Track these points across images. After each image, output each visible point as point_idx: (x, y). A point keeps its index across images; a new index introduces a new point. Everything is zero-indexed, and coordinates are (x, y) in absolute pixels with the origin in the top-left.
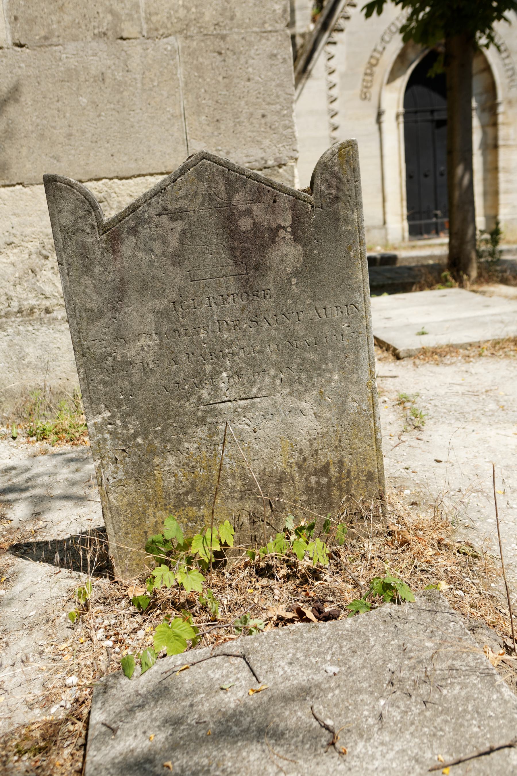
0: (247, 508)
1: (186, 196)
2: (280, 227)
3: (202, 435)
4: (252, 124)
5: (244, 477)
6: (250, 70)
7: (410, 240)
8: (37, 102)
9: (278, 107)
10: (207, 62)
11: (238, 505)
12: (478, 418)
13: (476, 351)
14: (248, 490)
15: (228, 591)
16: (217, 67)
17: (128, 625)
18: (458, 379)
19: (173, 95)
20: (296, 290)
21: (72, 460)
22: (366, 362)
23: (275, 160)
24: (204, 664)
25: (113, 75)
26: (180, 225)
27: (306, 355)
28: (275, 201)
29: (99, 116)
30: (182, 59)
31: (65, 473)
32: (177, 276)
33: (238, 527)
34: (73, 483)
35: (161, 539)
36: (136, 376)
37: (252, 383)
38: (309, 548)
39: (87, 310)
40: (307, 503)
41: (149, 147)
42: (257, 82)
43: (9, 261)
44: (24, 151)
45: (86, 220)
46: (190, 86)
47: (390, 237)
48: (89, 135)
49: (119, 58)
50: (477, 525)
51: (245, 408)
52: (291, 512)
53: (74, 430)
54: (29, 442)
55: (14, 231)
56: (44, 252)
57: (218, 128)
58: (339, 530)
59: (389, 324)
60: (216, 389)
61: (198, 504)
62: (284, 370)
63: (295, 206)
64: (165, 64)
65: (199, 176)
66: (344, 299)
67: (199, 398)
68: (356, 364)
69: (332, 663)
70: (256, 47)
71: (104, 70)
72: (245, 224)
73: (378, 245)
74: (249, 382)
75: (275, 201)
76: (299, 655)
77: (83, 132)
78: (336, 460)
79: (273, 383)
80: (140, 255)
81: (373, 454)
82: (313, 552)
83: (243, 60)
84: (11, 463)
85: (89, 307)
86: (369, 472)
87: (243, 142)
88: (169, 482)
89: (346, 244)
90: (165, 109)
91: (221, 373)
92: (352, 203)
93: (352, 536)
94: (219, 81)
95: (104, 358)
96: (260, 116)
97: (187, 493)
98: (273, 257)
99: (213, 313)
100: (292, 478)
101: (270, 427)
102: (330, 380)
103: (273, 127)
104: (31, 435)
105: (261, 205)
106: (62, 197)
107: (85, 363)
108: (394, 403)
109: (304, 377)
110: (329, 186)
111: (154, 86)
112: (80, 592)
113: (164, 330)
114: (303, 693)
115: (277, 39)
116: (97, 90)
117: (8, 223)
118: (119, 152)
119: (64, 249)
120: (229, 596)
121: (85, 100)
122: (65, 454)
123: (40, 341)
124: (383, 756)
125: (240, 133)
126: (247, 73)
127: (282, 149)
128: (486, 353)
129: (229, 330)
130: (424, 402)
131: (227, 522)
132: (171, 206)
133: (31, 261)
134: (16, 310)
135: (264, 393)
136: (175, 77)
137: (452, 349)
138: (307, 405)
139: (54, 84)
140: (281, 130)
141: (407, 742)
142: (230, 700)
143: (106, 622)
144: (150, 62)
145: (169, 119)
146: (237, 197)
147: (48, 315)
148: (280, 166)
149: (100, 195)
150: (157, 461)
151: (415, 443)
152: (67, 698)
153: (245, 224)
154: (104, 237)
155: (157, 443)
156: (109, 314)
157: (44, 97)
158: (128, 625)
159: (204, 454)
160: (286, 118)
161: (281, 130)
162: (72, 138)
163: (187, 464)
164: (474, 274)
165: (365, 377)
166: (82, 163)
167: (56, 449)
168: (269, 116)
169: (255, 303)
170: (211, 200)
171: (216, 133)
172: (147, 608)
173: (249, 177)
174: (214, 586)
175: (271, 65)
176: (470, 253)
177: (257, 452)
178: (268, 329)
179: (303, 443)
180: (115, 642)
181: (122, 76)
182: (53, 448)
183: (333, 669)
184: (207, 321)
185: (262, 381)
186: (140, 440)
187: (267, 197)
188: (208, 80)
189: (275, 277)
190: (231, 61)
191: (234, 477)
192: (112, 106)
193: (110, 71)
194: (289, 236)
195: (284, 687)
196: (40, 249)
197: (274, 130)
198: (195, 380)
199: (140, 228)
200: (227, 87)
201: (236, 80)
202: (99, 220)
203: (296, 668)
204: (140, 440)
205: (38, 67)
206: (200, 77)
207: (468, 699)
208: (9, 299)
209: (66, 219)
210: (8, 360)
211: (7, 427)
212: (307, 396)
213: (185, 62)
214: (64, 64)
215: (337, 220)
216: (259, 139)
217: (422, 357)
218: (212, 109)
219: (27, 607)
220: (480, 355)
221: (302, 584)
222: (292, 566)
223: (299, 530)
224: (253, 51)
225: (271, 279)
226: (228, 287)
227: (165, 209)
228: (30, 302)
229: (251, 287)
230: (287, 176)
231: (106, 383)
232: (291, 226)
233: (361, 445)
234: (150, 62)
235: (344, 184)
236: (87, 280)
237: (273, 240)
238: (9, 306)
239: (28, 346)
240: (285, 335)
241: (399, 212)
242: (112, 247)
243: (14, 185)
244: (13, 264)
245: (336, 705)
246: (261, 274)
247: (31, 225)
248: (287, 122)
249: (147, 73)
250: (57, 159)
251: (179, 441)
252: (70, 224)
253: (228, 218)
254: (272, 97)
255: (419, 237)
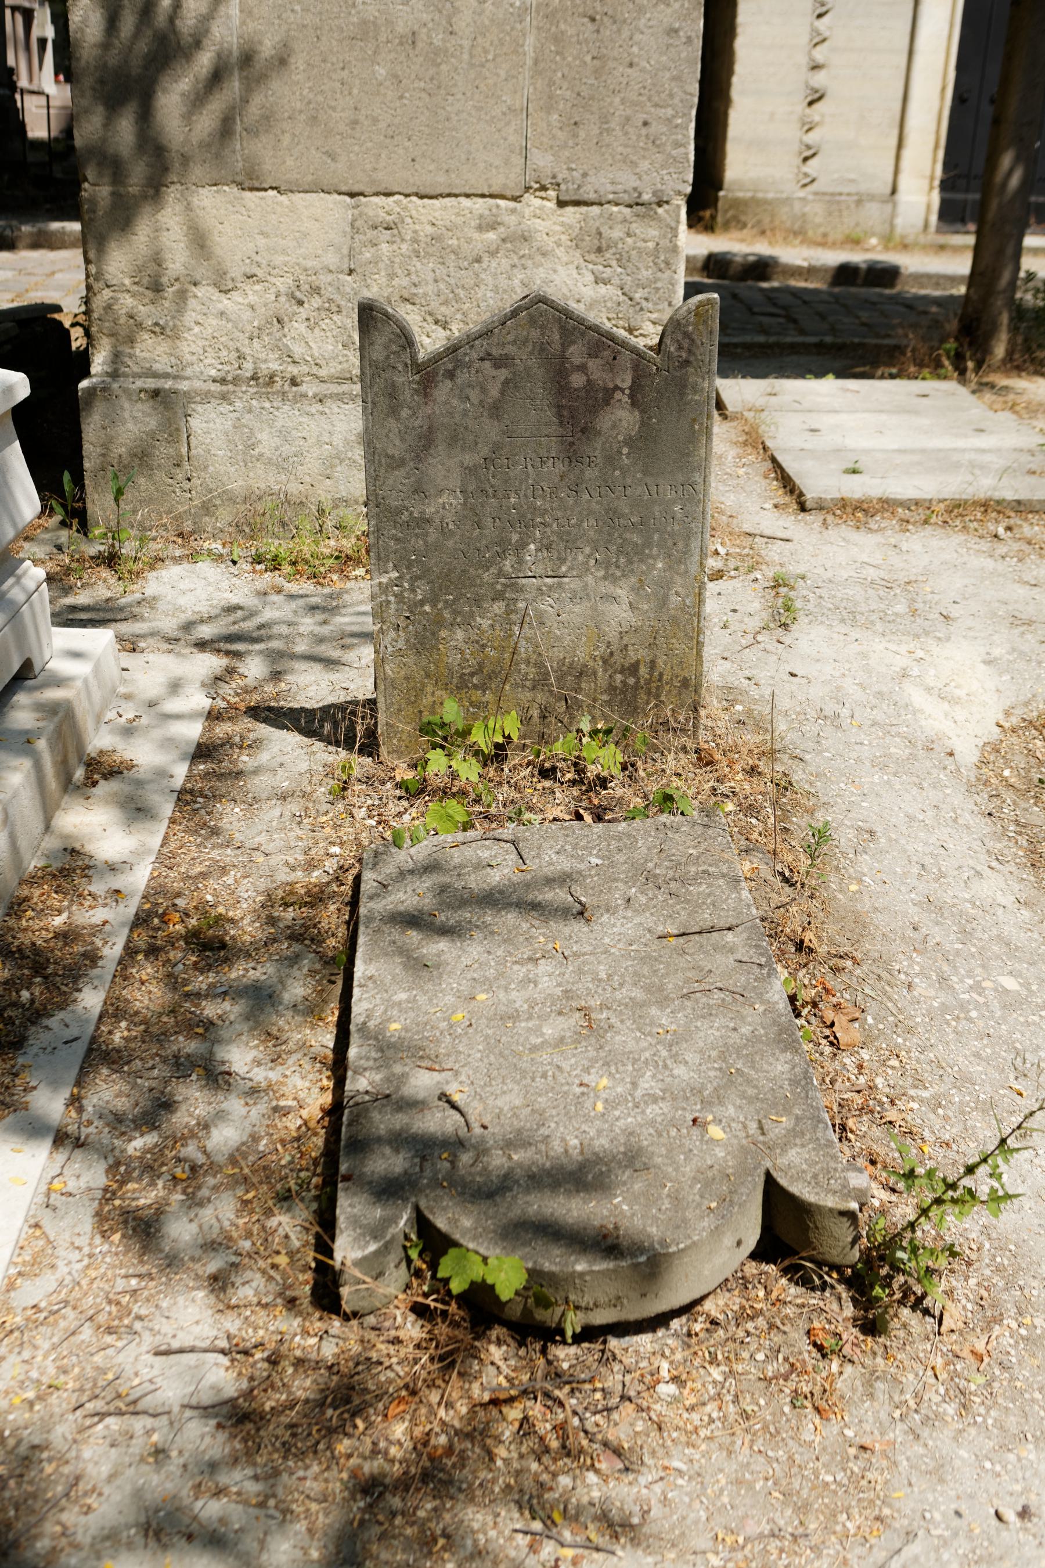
0: (539, 700)
1: (514, 342)
2: (617, 388)
3: (498, 612)
4: (626, 133)
5: (539, 665)
6: (635, 49)
7: (938, 231)
8: (313, 66)
9: (670, 112)
10: (571, 31)
11: (529, 695)
12: (872, 623)
13: (922, 513)
14: (541, 681)
15: (505, 787)
16: (586, 40)
17: (393, 808)
18: (877, 558)
19: (513, 77)
20: (626, 461)
21: (314, 608)
22: (698, 552)
23: (654, 193)
24: (474, 844)
25: (429, 37)
26: (503, 374)
27: (628, 536)
28: (615, 358)
29: (401, 97)
30: (534, 23)
31: (308, 624)
32: (492, 430)
33: (526, 720)
34: (321, 640)
35: (439, 721)
36: (433, 536)
37: (563, 560)
38: (601, 753)
39: (387, 456)
40: (608, 703)
41: (469, 153)
42: (643, 70)
43: (246, 302)
44: (286, 139)
45: (399, 357)
46: (542, 65)
47: (899, 221)
48: (382, 125)
49: (440, 12)
50: (807, 757)
51: (550, 588)
52: (589, 711)
53: (317, 562)
54: (254, 571)
55: (258, 258)
56: (298, 294)
57: (576, 136)
58: (640, 735)
59: (812, 443)
60: (521, 561)
61: (483, 688)
62: (601, 549)
63: (637, 366)
64: (508, 28)
65: (532, 321)
66: (680, 478)
67: (500, 570)
68: (685, 553)
69: (597, 856)
70: (648, 15)
71: (416, 28)
72: (577, 380)
73: (873, 234)
74: (559, 558)
75: (615, 358)
76: (568, 847)
77: (375, 120)
78: (648, 659)
79: (587, 563)
80: (455, 402)
81: (692, 659)
82: (604, 759)
83: (626, 33)
84: (235, 599)
85: (390, 453)
86: (685, 678)
87: (610, 161)
88: (454, 659)
89: (691, 416)
90: (499, 97)
91: (528, 544)
92: (704, 369)
93: (655, 749)
94: (585, 63)
95: (399, 512)
96: (640, 124)
97: (472, 674)
98: (605, 421)
99: (528, 476)
100: (595, 673)
101: (577, 612)
102: (653, 567)
103: (658, 142)
104: (258, 560)
105: (598, 361)
106: (375, 328)
107: (378, 515)
108: (767, 584)
109: (622, 560)
110: (680, 348)
111: (487, 61)
112: (344, 767)
113: (471, 489)
114: (564, 879)
115: (683, 5)
116: (402, 58)
117: (251, 245)
118: (423, 156)
119: (371, 386)
120: (504, 793)
121: (383, 72)
122: (307, 596)
123: (278, 424)
124: (622, 925)
125: (608, 146)
126: (629, 54)
127: (666, 178)
128: (934, 520)
129: (544, 498)
130: (808, 589)
131: (513, 713)
132: (495, 352)
133: (278, 305)
134: (249, 374)
135: (575, 573)
136: (521, 50)
137: (888, 505)
138: (622, 592)
139: (340, 41)
140: (669, 148)
141: (648, 919)
142: (496, 877)
143: (369, 802)
144: (487, 22)
145: (504, 114)
146: (571, 349)
147: (294, 389)
148: (659, 204)
149: (389, 218)
150: (443, 633)
151: (772, 646)
152: (331, 865)
153: (577, 380)
154: (417, 377)
155: (446, 614)
156: (412, 464)
157: (324, 61)
158: (393, 808)
159: (497, 632)
160: (678, 130)
161: (669, 148)
162: (358, 127)
163: (477, 642)
164: (1000, 350)
165: (694, 569)
166: (368, 167)
167: (293, 587)
168: (654, 124)
169: (577, 471)
170: (542, 350)
171: (571, 143)
172: (414, 792)
173: (589, 328)
174: (491, 781)
175: (668, 46)
176: (1000, 313)
177: (559, 639)
178: (588, 501)
179: (612, 635)
180: (379, 823)
181: (443, 40)
182: (290, 585)
183: (595, 861)
184: (521, 483)
185: (574, 559)
186: (427, 608)
187: (606, 353)
188: (570, 59)
189: (604, 444)
190: (608, 33)
191: (528, 662)
192: (422, 84)
193: (425, 30)
194: (626, 399)
195: (548, 871)
196: (294, 289)
197: (658, 146)
198: (498, 549)
199: (458, 371)
200: (597, 73)
201: (611, 64)
202: (413, 357)
203: (562, 857)
204: (427, 608)
205: (321, 13)
206: (557, 53)
207: (709, 895)
208: (241, 357)
209: (378, 353)
210: (232, 447)
211: (224, 544)
212: (623, 583)
213: (539, 28)
214: (359, 13)
215: (685, 386)
216: (635, 158)
217: (838, 512)
218: (569, 105)
219: (278, 777)
220: (926, 522)
221: (587, 791)
222: (580, 770)
223: (594, 733)
224: (643, 21)
225: (599, 446)
226: (548, 450)
227: (489, 354)
228: (271, 365)
229: (575, 453)
230: (669, 220)
231: (398, 540)
232: (630, 388)
233: (679, 647)
234: (487, 22)
235: (698, 347)
236: (391, 423)
237: (607, 402)
238: (240, 368)
239: (261, 430)
240: (607, 511)
241: (928, 173)
242: (425, 389)
243: (266, 190)
244: (252, 307)
245: (592, 888)
246: (588, 439)
247: (284, 252)
248: (680, 137)
249: (480, 40)
250: (332, 156)
251: (472, 615)
252: (381, 359)
253: (559, 372)
254: (663, 96)
255: (959, 226)
